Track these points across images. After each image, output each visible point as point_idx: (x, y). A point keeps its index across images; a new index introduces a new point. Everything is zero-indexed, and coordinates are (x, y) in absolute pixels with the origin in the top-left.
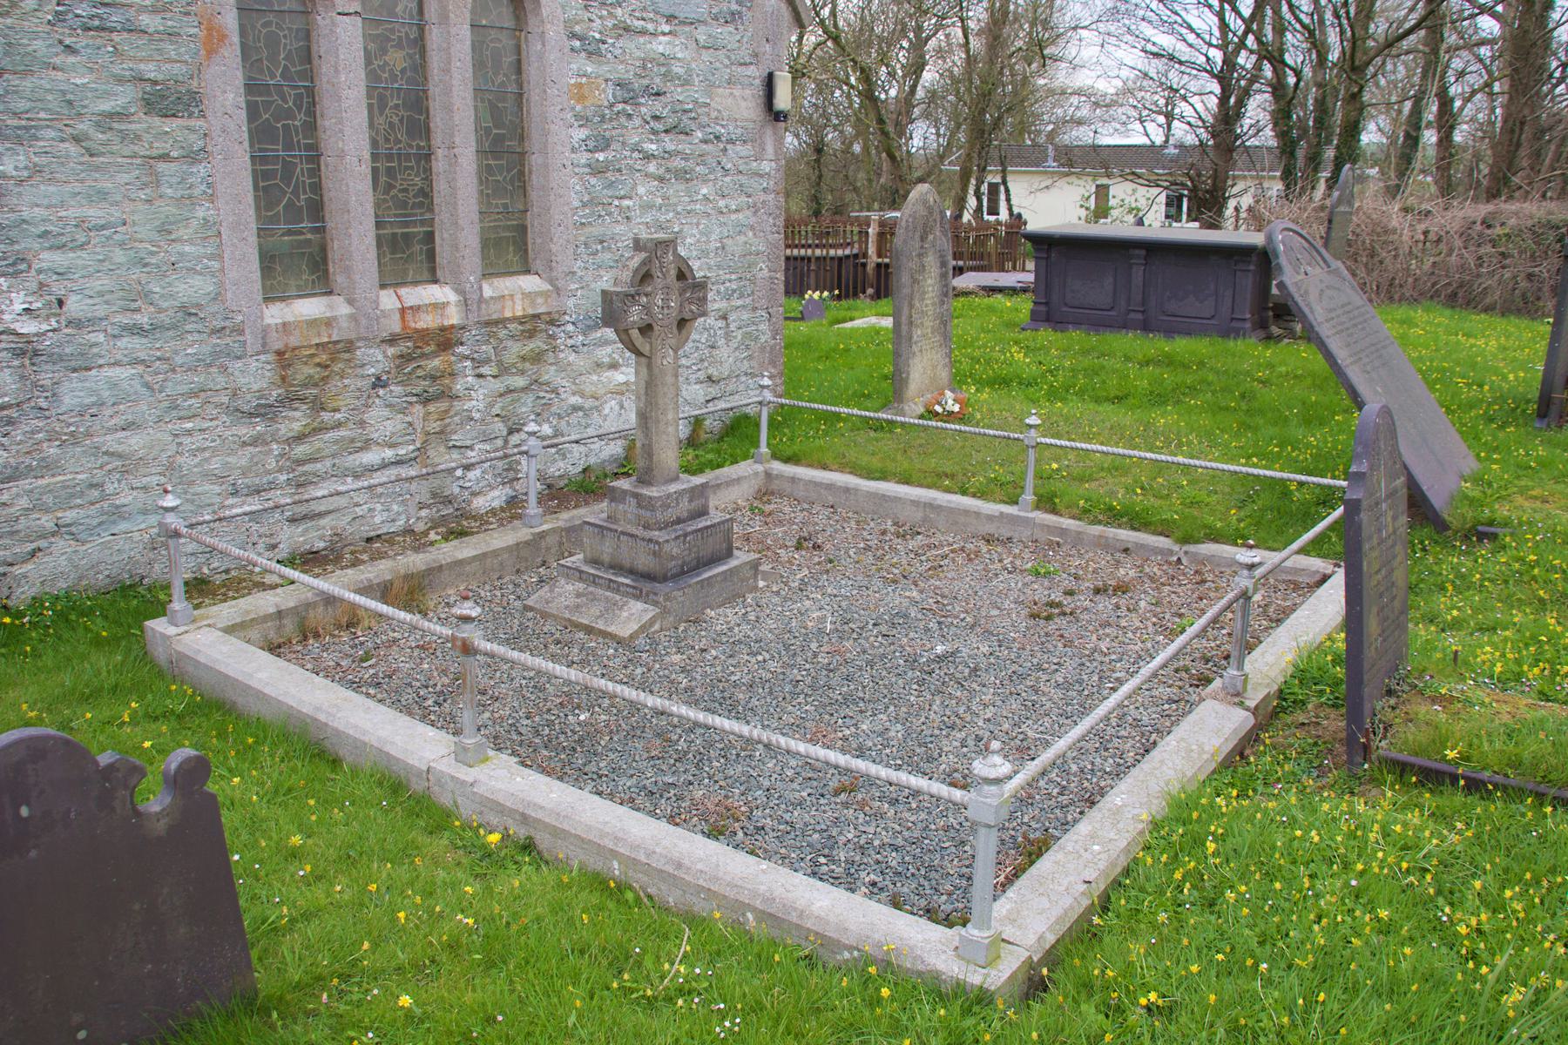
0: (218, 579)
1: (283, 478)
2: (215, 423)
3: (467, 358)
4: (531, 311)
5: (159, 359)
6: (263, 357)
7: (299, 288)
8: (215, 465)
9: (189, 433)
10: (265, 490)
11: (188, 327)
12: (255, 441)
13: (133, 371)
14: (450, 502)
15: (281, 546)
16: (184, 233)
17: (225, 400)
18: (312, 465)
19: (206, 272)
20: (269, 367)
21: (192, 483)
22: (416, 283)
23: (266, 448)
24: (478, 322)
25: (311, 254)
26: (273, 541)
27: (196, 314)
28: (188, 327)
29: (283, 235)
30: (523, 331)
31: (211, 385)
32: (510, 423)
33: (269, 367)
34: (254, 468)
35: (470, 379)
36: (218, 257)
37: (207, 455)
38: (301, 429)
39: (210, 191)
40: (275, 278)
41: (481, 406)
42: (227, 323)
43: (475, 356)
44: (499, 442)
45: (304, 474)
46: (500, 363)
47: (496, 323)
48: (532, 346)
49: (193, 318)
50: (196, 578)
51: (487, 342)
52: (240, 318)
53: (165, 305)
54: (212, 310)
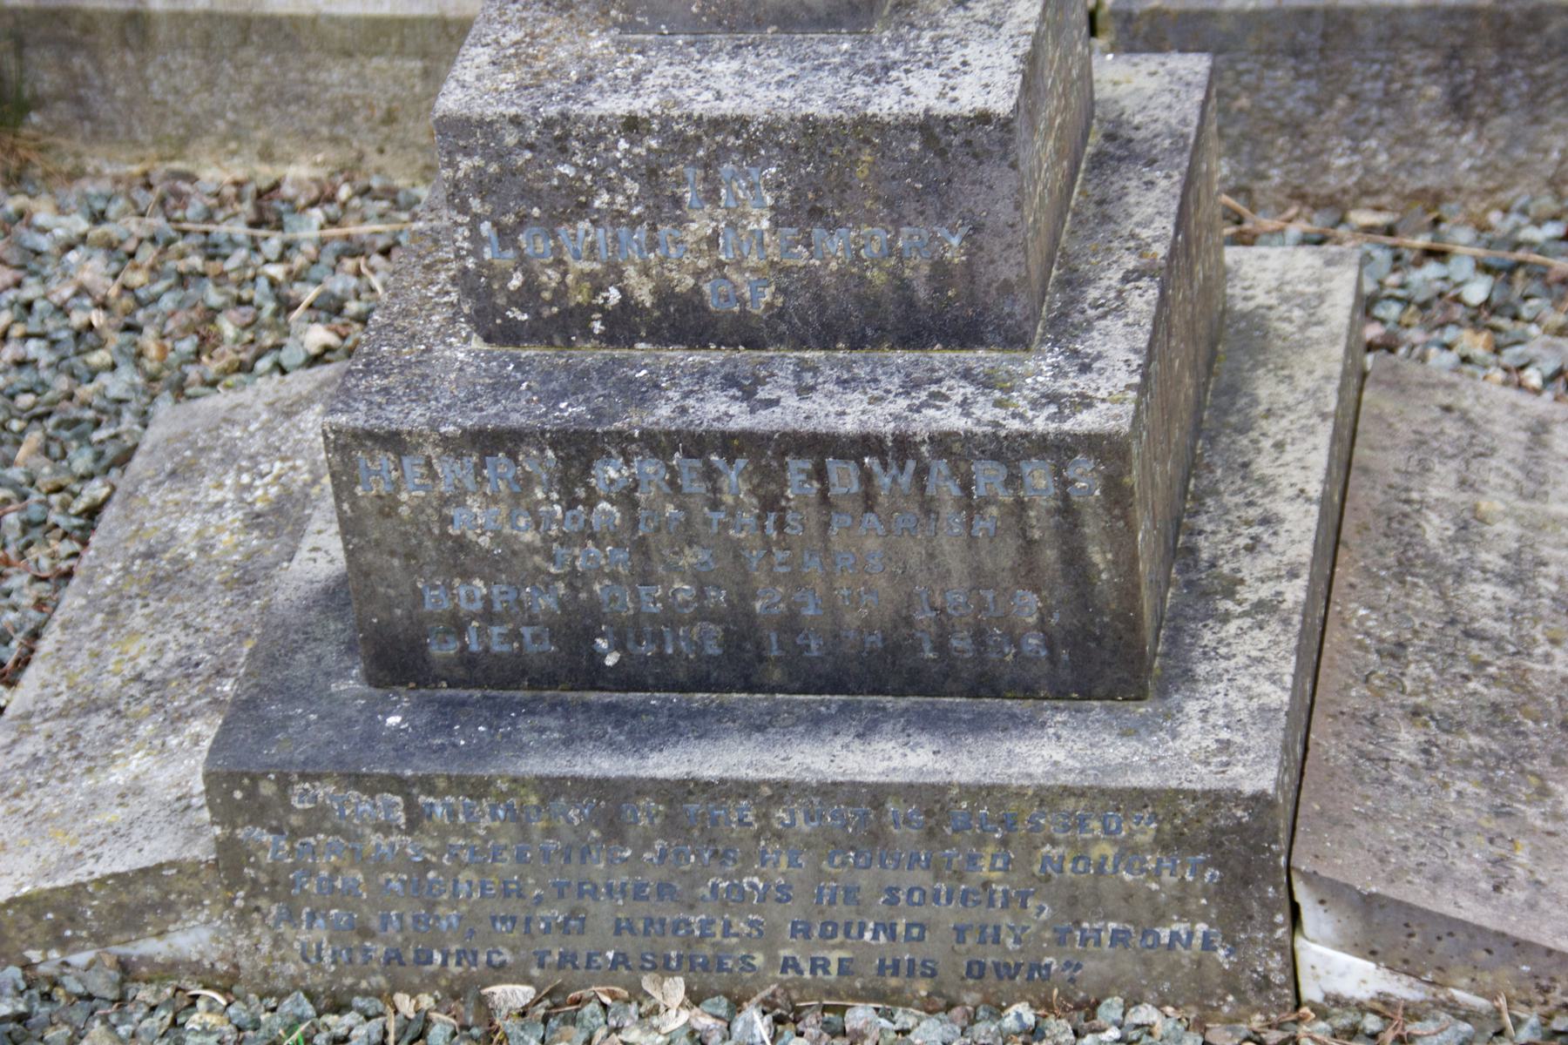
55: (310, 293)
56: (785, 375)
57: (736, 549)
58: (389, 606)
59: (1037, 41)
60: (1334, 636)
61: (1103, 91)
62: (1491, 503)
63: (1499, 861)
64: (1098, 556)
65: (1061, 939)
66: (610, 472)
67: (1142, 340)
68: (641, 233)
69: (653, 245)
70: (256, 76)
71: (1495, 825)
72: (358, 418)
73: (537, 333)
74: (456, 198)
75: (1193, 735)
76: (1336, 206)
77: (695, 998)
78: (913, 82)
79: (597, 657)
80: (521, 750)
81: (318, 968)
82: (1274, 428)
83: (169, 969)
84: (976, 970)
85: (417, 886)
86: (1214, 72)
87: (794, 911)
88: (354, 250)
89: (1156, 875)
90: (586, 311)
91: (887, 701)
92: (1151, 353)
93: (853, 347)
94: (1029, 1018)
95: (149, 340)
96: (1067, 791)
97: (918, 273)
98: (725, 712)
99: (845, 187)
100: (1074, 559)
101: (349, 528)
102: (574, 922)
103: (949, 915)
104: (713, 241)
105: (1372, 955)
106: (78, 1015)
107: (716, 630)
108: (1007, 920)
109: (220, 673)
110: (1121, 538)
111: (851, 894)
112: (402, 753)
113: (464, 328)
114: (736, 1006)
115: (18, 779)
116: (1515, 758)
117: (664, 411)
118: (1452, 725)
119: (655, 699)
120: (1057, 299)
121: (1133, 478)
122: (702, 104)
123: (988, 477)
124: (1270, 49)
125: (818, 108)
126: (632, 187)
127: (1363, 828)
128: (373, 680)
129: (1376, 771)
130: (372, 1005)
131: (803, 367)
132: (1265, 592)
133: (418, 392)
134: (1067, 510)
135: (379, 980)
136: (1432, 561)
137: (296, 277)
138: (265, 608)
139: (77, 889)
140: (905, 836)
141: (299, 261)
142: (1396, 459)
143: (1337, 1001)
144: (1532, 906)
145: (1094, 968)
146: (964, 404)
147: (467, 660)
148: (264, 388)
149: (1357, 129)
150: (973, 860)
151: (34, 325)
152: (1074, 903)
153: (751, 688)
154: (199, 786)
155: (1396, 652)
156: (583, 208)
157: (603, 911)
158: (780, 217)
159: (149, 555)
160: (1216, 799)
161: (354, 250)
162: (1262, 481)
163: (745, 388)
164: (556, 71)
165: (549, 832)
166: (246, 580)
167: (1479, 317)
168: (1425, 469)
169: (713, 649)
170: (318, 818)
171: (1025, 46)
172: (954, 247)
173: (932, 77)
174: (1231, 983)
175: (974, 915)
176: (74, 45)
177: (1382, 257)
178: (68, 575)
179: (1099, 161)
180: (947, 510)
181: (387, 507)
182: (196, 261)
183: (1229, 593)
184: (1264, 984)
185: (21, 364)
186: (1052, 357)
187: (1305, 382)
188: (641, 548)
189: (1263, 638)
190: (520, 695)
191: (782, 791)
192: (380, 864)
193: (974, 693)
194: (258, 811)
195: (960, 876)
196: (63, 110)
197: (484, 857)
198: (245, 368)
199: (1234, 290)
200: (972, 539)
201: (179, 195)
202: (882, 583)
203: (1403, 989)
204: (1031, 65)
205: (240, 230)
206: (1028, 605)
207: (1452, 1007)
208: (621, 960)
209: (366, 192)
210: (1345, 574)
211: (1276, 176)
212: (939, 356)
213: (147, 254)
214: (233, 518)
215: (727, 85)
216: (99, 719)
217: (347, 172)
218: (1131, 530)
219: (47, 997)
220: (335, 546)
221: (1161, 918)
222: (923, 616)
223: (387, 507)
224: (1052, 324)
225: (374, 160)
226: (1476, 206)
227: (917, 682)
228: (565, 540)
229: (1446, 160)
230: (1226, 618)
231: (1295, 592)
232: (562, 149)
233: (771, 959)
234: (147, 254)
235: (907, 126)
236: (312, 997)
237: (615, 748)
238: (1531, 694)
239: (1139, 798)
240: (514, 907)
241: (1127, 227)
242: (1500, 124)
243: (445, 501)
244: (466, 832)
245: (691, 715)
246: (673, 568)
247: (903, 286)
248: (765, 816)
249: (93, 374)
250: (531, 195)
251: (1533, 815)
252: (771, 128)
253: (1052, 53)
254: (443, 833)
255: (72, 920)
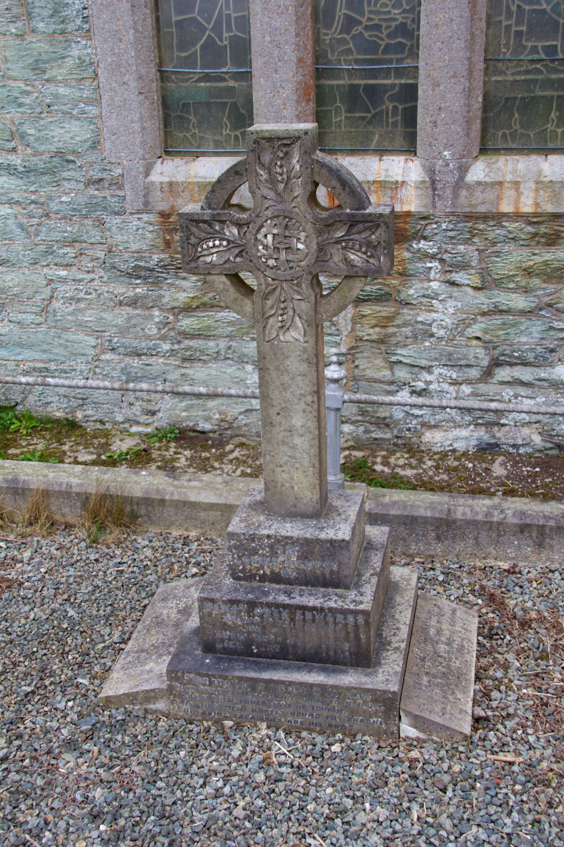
0: (90, 427)
1: (166, 346)
2: (91, 276)
3: (433, 257)
4: (549, 208)
5: (33, 202)
6: (145, 217)
7: (217, 143)
8: (89, 317)
9: (63, 280)
10: (145, 354)
11: (65, 175)
12: (134, 302)
13: (10, 211)
14: (387, 425)
15: (160, 415)
16: (58, 73)
17: (101, 255)
18: (201, 342)
19: (82, 117)
20: (151, 228)
21: (66, 330)
22: (381, 152)
23: (147, 313)
24: (452, 214)
25: (234, 105)
26: (150, 408)
27: (73, 161)
28: (65, 175)
29: (199, 80)
30: (535, 235)
31: (85, 237)
32: (497, 352)
33: (151, 228)
34: (132, 330)
35: (435, 285)
36: (96, 101)
37: (82, 305)
38: (186, 300)
39: (86, 26)
40: (188, 130)
41: (448, 321)
42: (105, 175)
43: (446, 256)
44: (474, 373)
45: (189, 349)
46: (484, 273)
47: (485, 217)
48: (548, 257)
49: (71, 166)
50: (67, 419)
51: (467, 242)
52: (119, 171)
53: (42, 148)
54: (90, 160)
55: (194, 561)
56: (297, 592)
57: (284, 629)
58: (209, 635)
59: (355, 524)
60: (411, 655)
61: (367, 533)
62: (444, 627)
63: (444, 708)
64: (362, 636)
65: (349, 720)
66: (258, 610)
67: (374, 589)
68: (268, 559)
69: (271, 562)
70: (186, 513)
71: (443, 700)
72: (205, 595)
73: (244, 579)
74: (230, 549)
75: (380, 677)
76: (412, 557)
77: (268, 727)
78: (328, 531)
79: (252, 650)
80: (235, 670)
81: (187, 714)
82: (400, 608)
83: (155, 712)
84: (330, 726)
85: (210, 698)
86: (390, 532)
87: (291, 710)
88: (203, 551)
89: (371, 707)
90: (255, 575)
91: (315, 664)
92: (376, 592)
93: (312, 586)
94: (341, 737)
95: (159, 568)
96: (353, 688)
97: (327, 572)
98: (279, 665)
99: (313, 553)
100: (357, 637)
101: (201, 618)
102: (243, 709)
103: (325, 713)
104: (284, 562)
105: (416, 728)
106: (135, 720)
107: (278, 646)
108: (338, 715)
109: (170, 646)
110: (368, 633)
111: (304, 707)
112: (209, 669)
113: (229, 576)
114: (277, 730)
115: (126, 666)
116: (448, 685)
117: (271, 598)
118: (435, 677)
119: (264, 660)
120: (356, 579)
121: (371, 620)
122: (284, 533)
123: (340, 617)
124: (400, 523)
125: (308, 536)
126: (267, 549)
127: (415, 699)
128: (203, 651)
129: (418, 686)
130: (198, 723)
131: (301, 590)
132: (397, 645)
133: (219, 590)
134: (356, 626)
135: (200, 718)
136: (431, 639)
137: (191, 557)
138: (181, 632)
139: (137, 692)
140: (317, 695)
141: (192, 553)
142: (424, 615)
143: (408, 737)
144: (450, 719)
145: (356, 727)
146: (336, 601)
147: (224, 649)
148: (182, 582)
149: (417, 542)
150: (331, 701)
151: (136, 564)
152: (353, 712)
153: (285, 659)
154: (164, 671)
155: (423, 659)
156: (257, 553)
157: (250, 707)
158: (299, 558)
159: (157, 617)
160: (385, 692)
161: (203, 551)
162: (397, 620)
163: (288, 594)
164: (253, 524)
165: (240, 688)
166: (177, 625)
167: (442, 583)
168: (430, 618)
169: (278, 650)
170: (190, 681)
171: (352, 525)
172: (335, 567)
173: (333, 531)
174: (385, 732)
175: (331, 713)
176: (149, 505)
177: (422, 569)
178: (139, 620)
179: (366, 549)
180: (330, 624)
181: (210, 614)
182: (170, 552)
183: (389, 645)
184: (392, 733)
185: (132, 572)
186: (355, 592)
187: (407, 598)
188: (264, 627)
189: (396, 655)
190: (235, 657)
191: (291, 683)
192: (202, 692)
193: (333, 664)
194: (177, 679)
195: (328, 705)
196: (146, 518)
197: (225, 693)
198: (179, 576)
199: (392, 576)
200: (335, 631)
201: (168, 538)
202: (315, 639)
203: (422, 736)
204: (354, 529)
205: (180, 546)
206: (347, 646)
207: (432, 740)
208: (253, 717)
209: (207, 539)
210: (413, 641)
211: (400, 549)
212: (330, 590)
213: (160, 550)
214: (175, 611)
215: (289, 529)
216: (144, 654)
217: (203, 534)
218: (370, 631)
219: (129, 716)
220: (197, 620)
221: (371, 717)
222: (324, 646)
223: (210, 614)
224: (355, 585)
225: (209, 532)
226: (441, 559)
227: (321, 660)
228: (247, 624)
229: (435, 549)
230: (388, 650)
231: (403, 645)
232: (253, 541)
233: (286, 720)
234: (160, 550)
235: (327, 541)
236: (185, 720)
237: (255, 671)
238: (451, 670)
239: (368, 690)
240: (231, 704)
241: (372, 564)
242: (446, 542)
243: (222, 614)
244: (222, 687)
245: (272, 664)
246: (270, 632)
247: (324, 575)
248: (287, 689)
249: (147, 575)
250: (245, 549)
251: (451, 698)
252: (298, 539)
253: (358, 526)
254: (217, 687)
255: (136, 699)
